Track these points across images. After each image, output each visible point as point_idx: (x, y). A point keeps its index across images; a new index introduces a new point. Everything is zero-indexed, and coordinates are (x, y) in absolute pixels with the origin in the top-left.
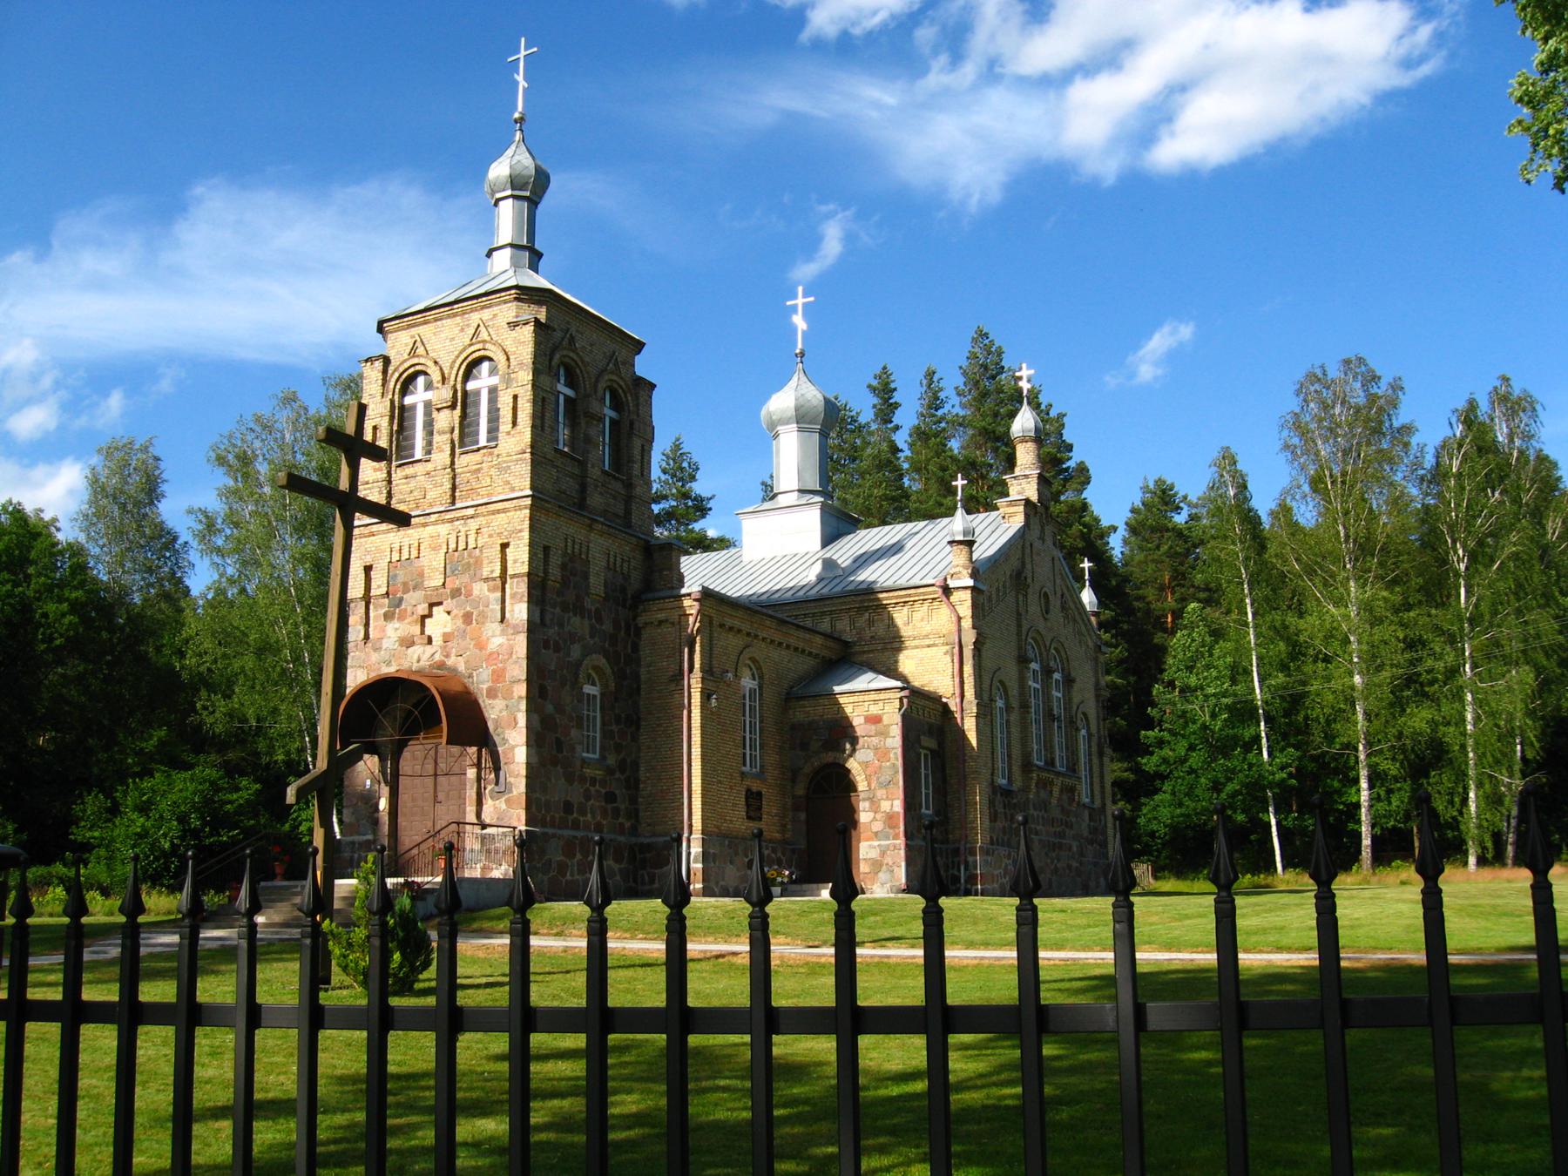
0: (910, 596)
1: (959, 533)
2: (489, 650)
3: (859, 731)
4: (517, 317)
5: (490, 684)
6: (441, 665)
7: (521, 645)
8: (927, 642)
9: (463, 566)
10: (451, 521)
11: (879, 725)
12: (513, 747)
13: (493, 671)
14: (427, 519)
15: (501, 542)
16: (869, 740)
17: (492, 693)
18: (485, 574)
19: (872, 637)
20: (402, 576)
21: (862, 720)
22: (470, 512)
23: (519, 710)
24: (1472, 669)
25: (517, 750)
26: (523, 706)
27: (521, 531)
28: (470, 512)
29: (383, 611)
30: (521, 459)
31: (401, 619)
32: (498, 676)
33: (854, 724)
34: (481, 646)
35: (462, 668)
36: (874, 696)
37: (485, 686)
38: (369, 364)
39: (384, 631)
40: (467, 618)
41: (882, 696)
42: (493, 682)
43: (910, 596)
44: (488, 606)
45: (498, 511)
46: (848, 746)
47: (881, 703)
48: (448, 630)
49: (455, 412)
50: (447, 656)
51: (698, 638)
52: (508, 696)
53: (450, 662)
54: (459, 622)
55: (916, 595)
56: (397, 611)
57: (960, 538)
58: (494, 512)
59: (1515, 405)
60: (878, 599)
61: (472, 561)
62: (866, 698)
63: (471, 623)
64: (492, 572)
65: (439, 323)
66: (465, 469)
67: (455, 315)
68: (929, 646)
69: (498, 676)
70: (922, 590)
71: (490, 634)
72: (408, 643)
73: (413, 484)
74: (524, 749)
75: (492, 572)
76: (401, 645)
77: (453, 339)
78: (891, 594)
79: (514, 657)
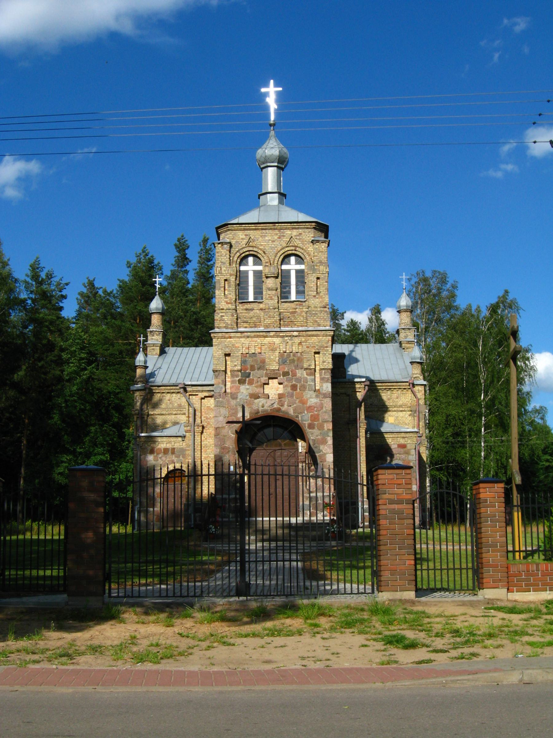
0: (393, 386)
1: (418, 358)
2: (308, 405)
3: (394, 451)
4: (314, 237)
5: (309, 422)
6: (279, 410)
7: (328, 404)
8: (401, 409)
9: (290, 360)
10: (283, 337)
11: (405, 449)
12: (325, 454)
13: (312, 416)
14: (268, 334)
15: (314, 351)
16: (400, 456)
17: (311, 426)
18: (305, 366)
19: (371, 404)
20: (250, 361)
21: (396, 446)
22: (295, 334)
23: (328, 436)
24: (485, 430)
25: (327, 455)
26: (331, 434)
27: (327, 347)
28: (295, 334)
29: (237, 379)
30: (324, 311)
31: (250, 383)
32: (315, 418)
33: (392, 448)
34: (303, 402)
35: (291, 412)
36: (403, 435)
37: (306, 423)
38: (220, 245)
39: (239, 389)
40: (294, 387)
41: (407, 435)
42: (311, 421)
43: (393, 386)
44: (307, 383)
45: (313, 336)
46: (388, 458)
47: (406, 439)
48: (281, 392)
49: (277, 280)
50: (282, 405)
51: (363, 404)
52: (321, 427)
53: (284, 408)
54: (289, 389)
55: (396, 386)
56: (247, 379)
57: (419, 361)
58: (310, 336)
59: (512, 306)
60: (376, 386)
61: (296, 358)
62: (399, 436)
63: (296, 390)
64: (310, 366)
65: (264, 231)
66: (286, 311)
67: (275, 229)
68: (401, 411)
69: (315, 418)
70: (399, 384)
71: (309, 396)
72: (255, 396)
73: (252, 314)
74: (332, 455)
75: (310, 366)
76: (251, 398)
77: (273, 241)
78: (383, 384)
79: (324, 409)
